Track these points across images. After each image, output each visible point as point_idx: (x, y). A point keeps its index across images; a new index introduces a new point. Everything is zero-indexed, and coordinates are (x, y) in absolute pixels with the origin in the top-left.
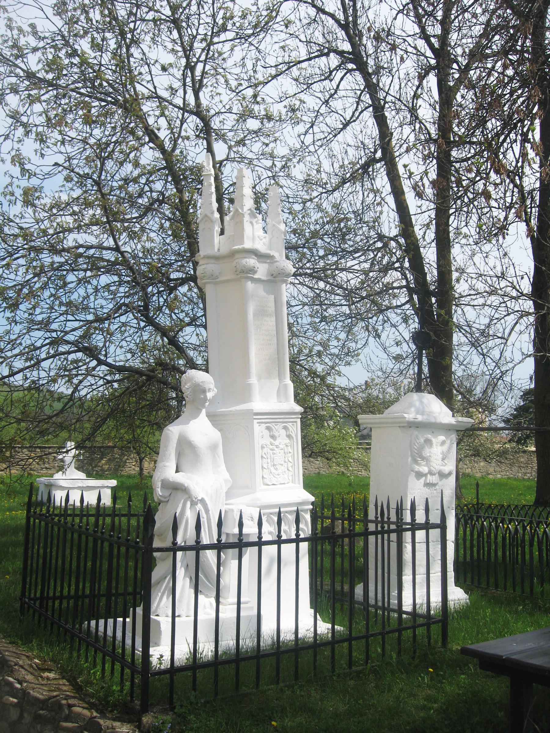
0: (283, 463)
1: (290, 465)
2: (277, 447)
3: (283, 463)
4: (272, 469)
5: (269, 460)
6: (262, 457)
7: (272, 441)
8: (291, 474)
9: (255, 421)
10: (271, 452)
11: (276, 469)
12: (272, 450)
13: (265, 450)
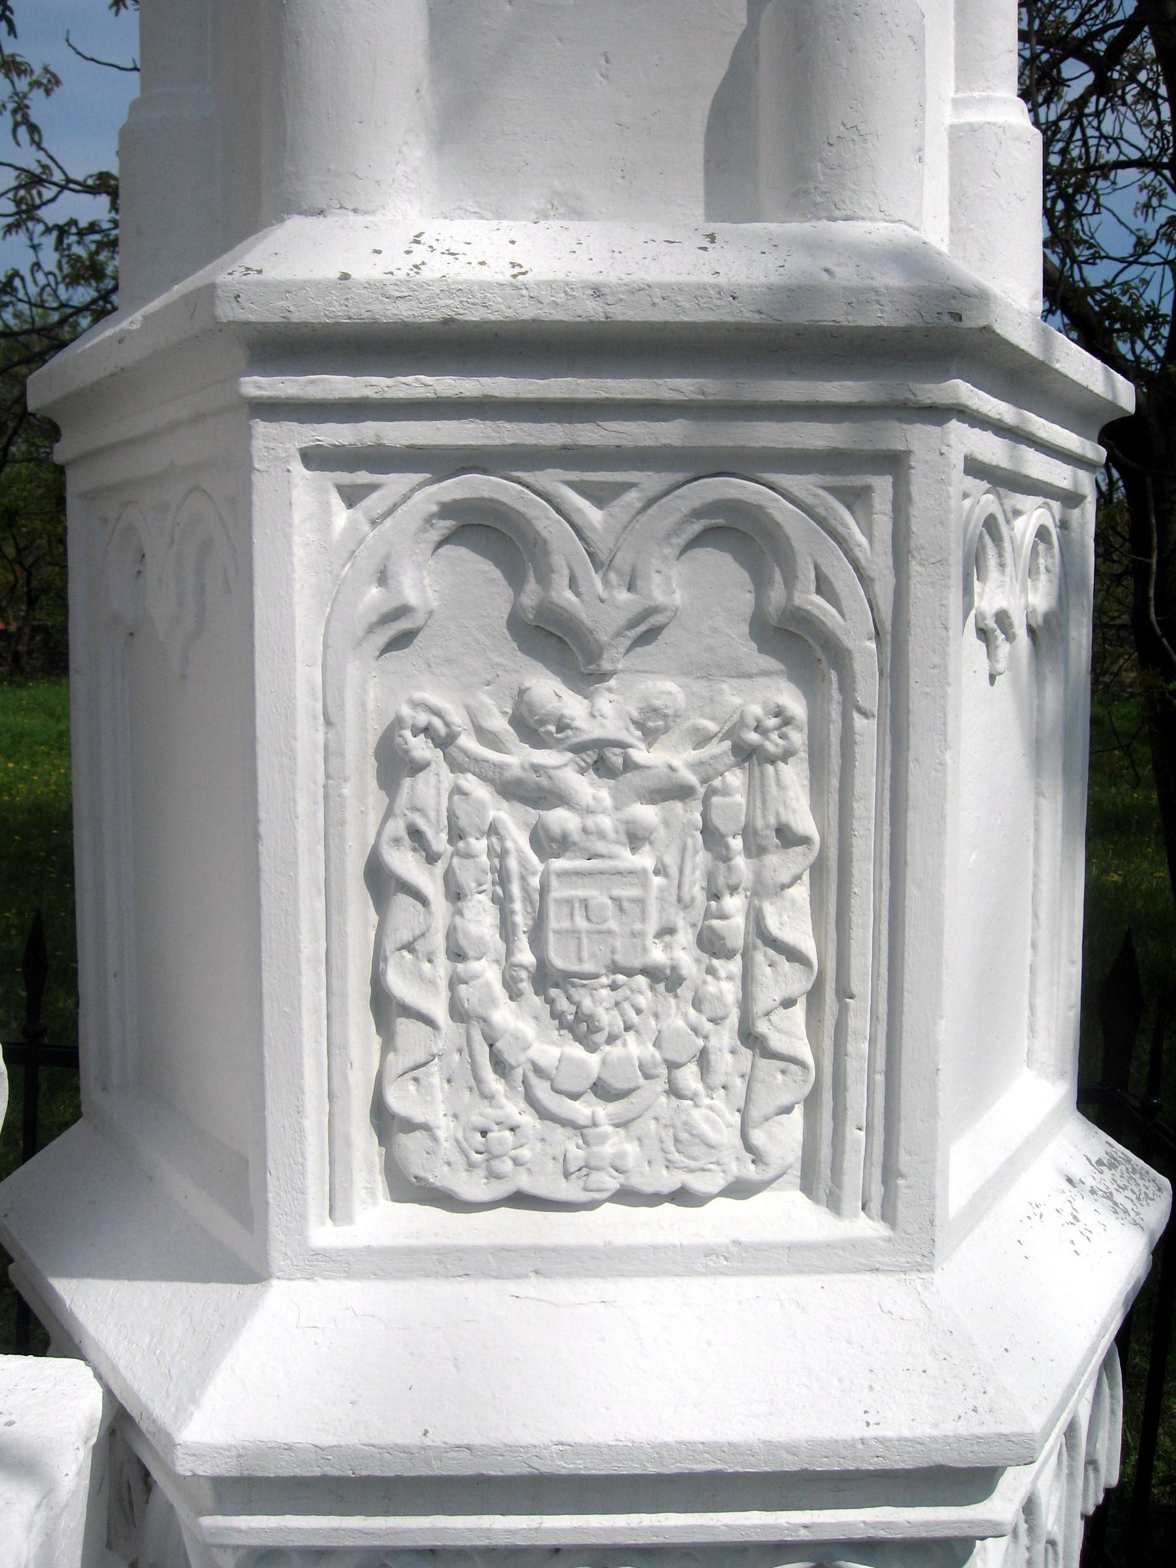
0: (683, 953)
1: (778, 981)
2: (601, 759)
3: (683, 953)
4: (518, 1021)
5: (480, 919)
6: (381, 882)
7: (548, 689)
8: (780, 1086)
9: (276, 445)
10: (516, 826)
11: (582, 1029)
12: (532, 793)
13: (431, 789)
